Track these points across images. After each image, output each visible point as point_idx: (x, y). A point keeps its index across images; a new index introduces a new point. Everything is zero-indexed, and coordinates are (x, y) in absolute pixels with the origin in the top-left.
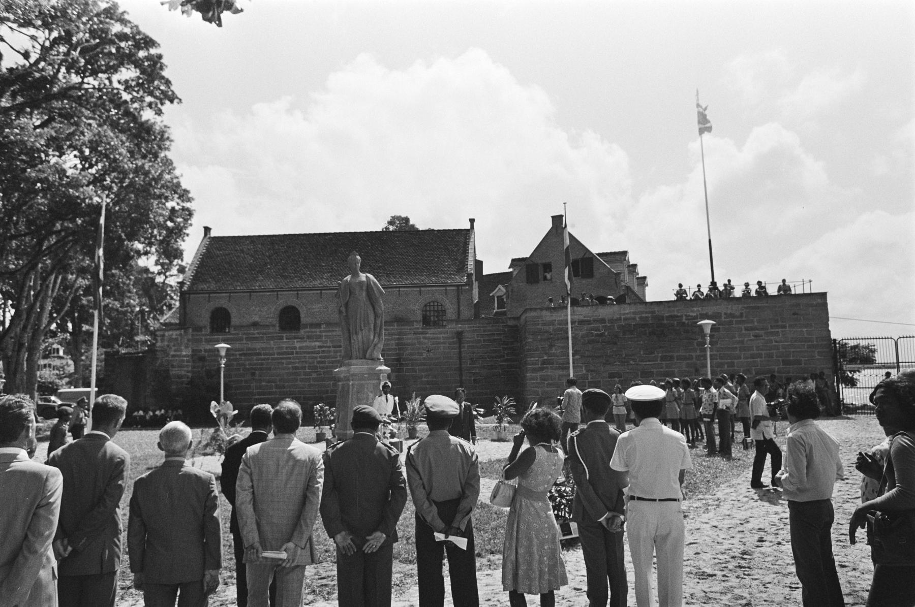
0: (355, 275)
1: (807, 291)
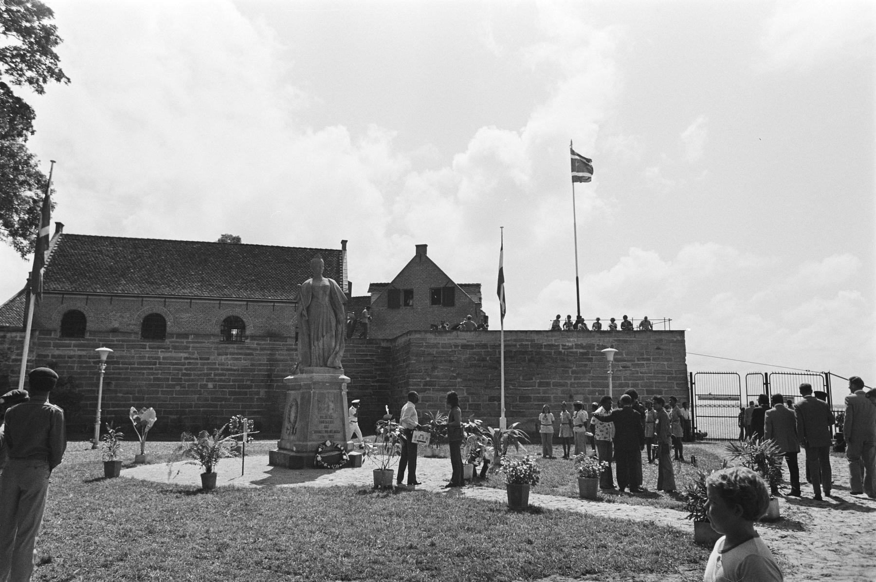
0: (317, 278)
1: (667, 329)
